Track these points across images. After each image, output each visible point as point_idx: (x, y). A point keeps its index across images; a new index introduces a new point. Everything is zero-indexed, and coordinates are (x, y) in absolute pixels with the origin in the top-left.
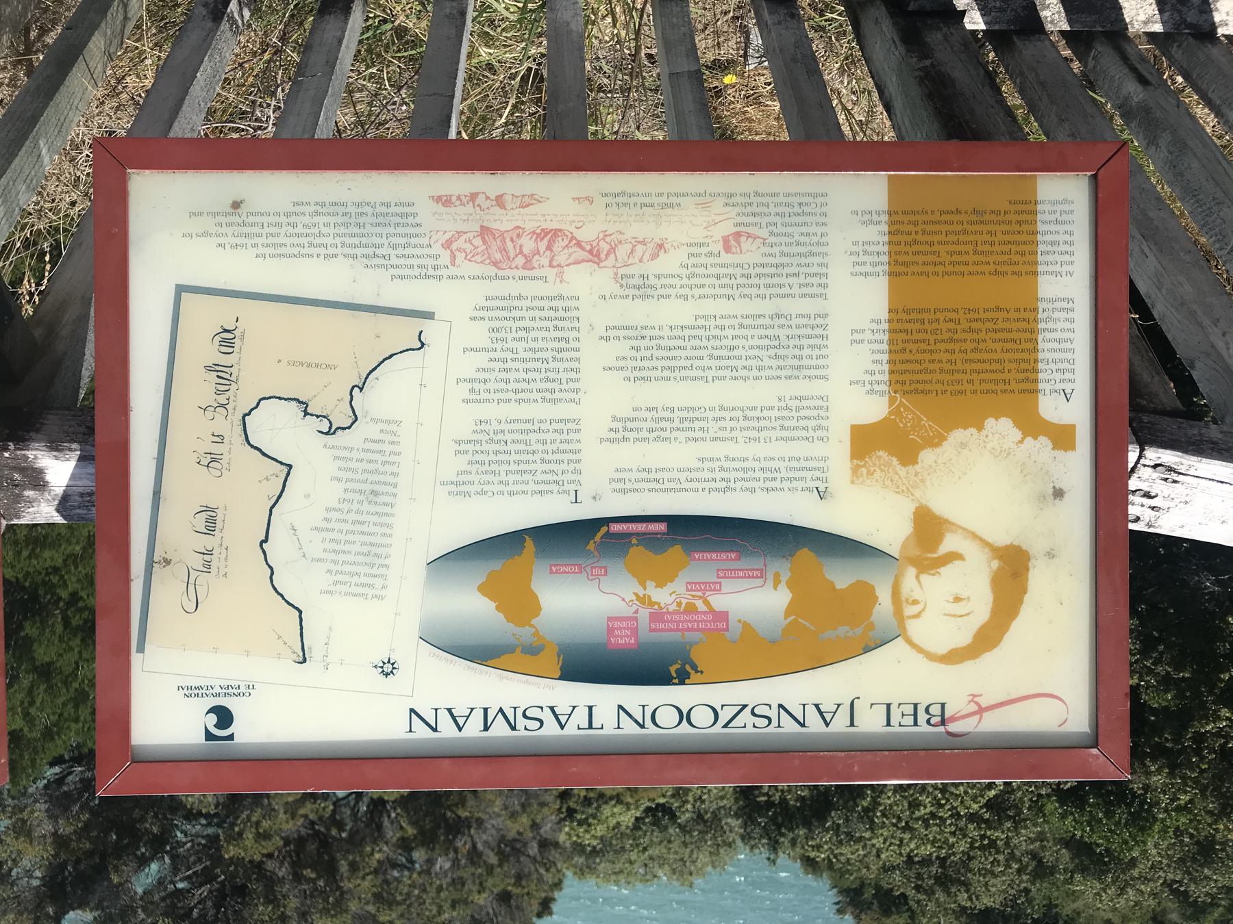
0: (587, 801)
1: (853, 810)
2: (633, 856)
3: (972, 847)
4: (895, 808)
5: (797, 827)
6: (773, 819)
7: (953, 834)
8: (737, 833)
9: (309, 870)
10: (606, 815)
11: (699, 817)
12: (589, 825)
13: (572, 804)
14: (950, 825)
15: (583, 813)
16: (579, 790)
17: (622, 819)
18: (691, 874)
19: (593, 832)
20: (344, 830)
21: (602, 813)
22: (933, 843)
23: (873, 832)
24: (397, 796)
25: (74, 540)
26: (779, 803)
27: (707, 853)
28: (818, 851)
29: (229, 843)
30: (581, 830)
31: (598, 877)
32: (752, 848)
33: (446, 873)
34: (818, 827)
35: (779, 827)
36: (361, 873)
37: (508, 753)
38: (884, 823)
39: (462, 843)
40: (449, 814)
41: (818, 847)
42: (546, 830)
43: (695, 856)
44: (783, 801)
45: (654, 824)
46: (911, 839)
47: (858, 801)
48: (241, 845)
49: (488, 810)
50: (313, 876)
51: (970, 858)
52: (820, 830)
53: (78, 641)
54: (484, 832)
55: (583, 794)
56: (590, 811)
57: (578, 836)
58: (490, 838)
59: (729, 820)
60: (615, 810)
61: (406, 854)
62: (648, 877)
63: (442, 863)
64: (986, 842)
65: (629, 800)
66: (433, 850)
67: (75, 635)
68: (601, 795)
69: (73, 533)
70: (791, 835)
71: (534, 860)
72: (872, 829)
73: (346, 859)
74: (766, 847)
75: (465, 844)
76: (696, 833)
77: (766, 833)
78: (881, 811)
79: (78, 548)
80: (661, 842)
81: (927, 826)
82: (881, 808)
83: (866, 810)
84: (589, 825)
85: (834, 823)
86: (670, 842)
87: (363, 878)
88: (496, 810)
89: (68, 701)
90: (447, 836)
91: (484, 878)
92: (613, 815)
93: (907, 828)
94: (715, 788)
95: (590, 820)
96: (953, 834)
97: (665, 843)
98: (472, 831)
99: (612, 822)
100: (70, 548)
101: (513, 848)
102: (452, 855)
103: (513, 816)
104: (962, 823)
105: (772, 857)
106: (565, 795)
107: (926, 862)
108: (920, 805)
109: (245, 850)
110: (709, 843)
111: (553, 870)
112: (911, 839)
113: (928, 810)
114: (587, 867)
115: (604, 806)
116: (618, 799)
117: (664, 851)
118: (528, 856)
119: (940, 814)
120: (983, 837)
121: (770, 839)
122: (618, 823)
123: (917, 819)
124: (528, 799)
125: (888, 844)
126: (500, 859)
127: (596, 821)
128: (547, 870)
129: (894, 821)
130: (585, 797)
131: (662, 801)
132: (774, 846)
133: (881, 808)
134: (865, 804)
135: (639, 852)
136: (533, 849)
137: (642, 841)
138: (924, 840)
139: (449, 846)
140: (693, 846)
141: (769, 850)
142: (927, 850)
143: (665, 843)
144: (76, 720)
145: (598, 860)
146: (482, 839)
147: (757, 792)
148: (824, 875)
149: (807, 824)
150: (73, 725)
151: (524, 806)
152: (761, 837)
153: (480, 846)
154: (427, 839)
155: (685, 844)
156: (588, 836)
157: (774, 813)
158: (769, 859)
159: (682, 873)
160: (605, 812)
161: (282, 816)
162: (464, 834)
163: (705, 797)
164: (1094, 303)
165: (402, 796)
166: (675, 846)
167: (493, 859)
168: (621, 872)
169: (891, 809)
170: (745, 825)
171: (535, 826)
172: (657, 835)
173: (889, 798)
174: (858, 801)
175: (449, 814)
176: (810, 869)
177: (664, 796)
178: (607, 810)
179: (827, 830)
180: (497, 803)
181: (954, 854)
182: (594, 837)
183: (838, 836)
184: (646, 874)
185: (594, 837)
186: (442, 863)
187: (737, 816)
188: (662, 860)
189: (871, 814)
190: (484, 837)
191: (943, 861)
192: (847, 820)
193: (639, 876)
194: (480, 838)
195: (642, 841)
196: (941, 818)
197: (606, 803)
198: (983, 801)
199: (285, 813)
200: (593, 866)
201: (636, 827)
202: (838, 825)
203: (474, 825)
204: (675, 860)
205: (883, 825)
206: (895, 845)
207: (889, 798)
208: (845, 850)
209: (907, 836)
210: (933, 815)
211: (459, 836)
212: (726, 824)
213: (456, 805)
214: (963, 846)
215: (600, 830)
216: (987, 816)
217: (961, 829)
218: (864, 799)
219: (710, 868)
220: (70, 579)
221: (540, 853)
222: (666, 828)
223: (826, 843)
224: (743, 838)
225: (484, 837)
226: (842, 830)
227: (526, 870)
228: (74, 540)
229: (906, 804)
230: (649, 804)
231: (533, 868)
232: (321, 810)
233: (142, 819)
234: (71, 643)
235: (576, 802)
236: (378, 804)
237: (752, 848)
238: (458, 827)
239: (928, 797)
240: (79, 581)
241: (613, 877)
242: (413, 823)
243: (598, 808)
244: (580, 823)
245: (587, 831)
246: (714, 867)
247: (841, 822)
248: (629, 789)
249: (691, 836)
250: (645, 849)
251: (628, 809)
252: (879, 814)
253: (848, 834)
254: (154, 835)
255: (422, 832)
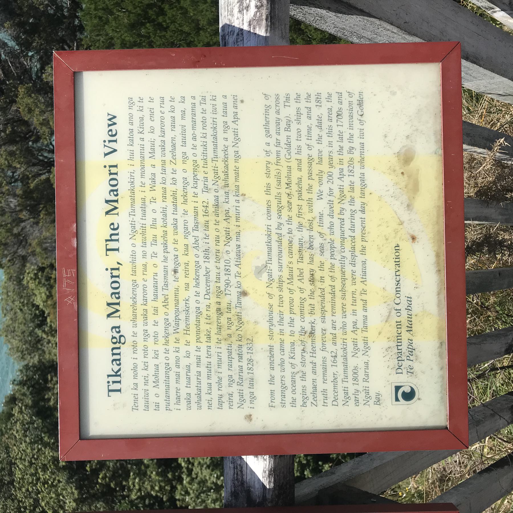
0: (48, 279)
1: (42, 432)
2: (17, 303)
3: (19, 501)
4: (43, 456)
5: (33, 397)
6: (38, 383)
7: (28, 490)
8: (29, 361)
9: (10, 130)
10: (41, 289)
11: (39, 341)
12: (35, 279)
13: (46, 271)
14: (33, 489)
15: (42, 276)
16: (55, 274)
17: (39, 298)
18: (6, 336)
19: (31, 282)
20: (33, 143)
21: (41, 287)
22: (23, 479)
23: (29, 443)
24: (52, 182)
25: (195, 12)
26: (46, 387)
27: (18, 345)
28: (19, 412)
29: (26, 88)
30: (32, 275)
31: (5, 283)
32: (21, 371)
33: (8, 205)
34: (33, 412)
35: (33, 386)
36: (9, 158)
37: (79, 282)
38: (34, 449)
39: (24, 215)
40: (42, 206)
41: (21, 412)
42: (31, 258)
43: (16, 338)
44: (49, 389)
45: (35, 314)
46: (25, 465)
47: (48, 434)
48: (24, 96)
49: (44, 228)
50: (7, 132)
51: (13, 500)
52: (31, 413)
53: (139, 12)
54: (31, 226)
55: (53, 276)
56: (43, 281)
57: (28, 273)
58: (28, 230)
59: (37, 357)
60: (43, 295)
61: (19, 179)
62: (5, 311)
63: (13, 202)
64: (22, 509)
65: (49, 302)
66: (22, 198)
67: (143, 11)
68: (51, 287)
69: (199, 12)
70: (28, 393)
71: (15, 252)
72: (31, 443)
73: (17, 150)
74: (22, 379)
75: (24, 216)
76: (30, 339)
77: (29, 379)
78: (41, 448)
79: (192, 14)
80: (25, 319)
81: (32, 475)
82: (43, 449)
83: (42, 439)
84: (35, 279)
85: (35, 421)
86: (25, 324)
87: (6, 159)
88: (44, 233)
89: (107, 5)
90: (29, 206)
91: (5, 228)
92: (40, 293)
93: (31, 463)
94: (57, 359)
95: (37, 280)
96: (28, 490)
97: (24, 322)
98: (32, 220)
99: (36, 292)
100: (191, 10)
101: (22, 241)
102: (18, 208)
103: (40, 244)
104: (33, 495)
105: (16, 382)
106: (52, 267)
107: (11, 474)
108: (45, 472)
109: (22, 98)
110: (24, 346)
111: (9, 264)
112: (25, 465)
113: (41, 476)
114: (11, 276)
115: (45, 288)
116: (50, 296)
117: (20, 321)
118: (18, 249)
119: (39, 484)
120: (25, 508)
121: (26, 381)
122: (36, 295)
123: (37, 469)
124: (49, 251)
125: (22, 452)
126: (16, 234)
127: (37, 283)
128: (9, 261)
129: (35, 456)
130: (51, 278)
131: (48, 320)
132: (22, 383)
133: (43, 449)
134: (46, 439)
135: (20, 306)
136: (21, 252)
137: (26, 308)
138: (24, 472)
139: (24, 207)
140: (22, 337)
141: (20, 381)
142: (18, 475)
143: (24, 322)
144: (95, 9)
145: (15, 283)
146: (27, 225)
147: (53, 374)
148: (5, 408)
149: (35, 404)
150: (93, 6)
151: (46, 249)
152: (27, 376)
153: (23, 224)
154: (27, 194)
155: (23, 332)
156: (29, 279)
157: (41, 383)
158: (14, 380)
159: (7, 331)
160: (42, 288)
161: (41, 118)
162: (29, 215)
163: (50, 345)
164: (288, 433)
165: (52, 185)
166: (22, 327)
167: (15, 231)
168: (8, 296)
169: (43, 454)
170: (34, 366)
171: (33, 253)
172: (29, 317)
173: (49, 453)
174: (48, 434)
175: (42, 206)
176: (7, 400)
177: (51, 322)
178: (43, 290)
179: (31, 418)
180: (48, 234)
181: (15, 491)
182: (28, 282)
183: (27, 424)
184: (6, 310)
185: (28, 282)
186: (13, 202)
187: (40, 361)
188: (14, 320)
189: (40, 442)
190: (28, 227)
191: (12, 482)
192: (36, 428)
193: (5, 306)
194: (28, 224)
195: (26, 308)
196: (37, 484)
197: (47, 289)
198: (46, 509)
199: (43, 120)
200: (12, 280)
201: (33, 305)
202: (33, 424)
203: (35, 220)
204: (14, 328)
205: (32, 449)
206: (22, 456)
207: (49, 453)
208: (18, 426)
209: (27, 464)
210: (38, 479)
211: (29, 213)
212: (35, 355)
213: (47, 210)
214: (20, 495)
215: (32, 285)
216: (37, 510)
217: (30, 494)
218: (49, 438)
219: (10, 346)
220: (174, 11)
221: (18, 256)
222: (33, 322)
223: (23, 417)
224: (27, 365)
225: (28, 227)
226: (31, 426)
227: (10, 249)
228: (195, 12)
229: (46, 462)
230: (47, 312)
231: (12, 251)
232: (44, 137)
233: (40, 38)
234: (138, 8)
235: (48, 272)
236: (49, 164)
237: (21, 371)
238: (34, 211)
239: (49, 476)
240: (173, 16)
241: (5, 291)
242: (37, 187)
243: (44, 285)
244: (36, 275)
245: (31, 278)
246: (10, 349)
247: (35, 425)
248: (55, 303)
249: (28, 336)
250: (21, 310)
251: (44, 302)
252: (40, 447)
253: (28, 429)
254: (32, 86)
255: (32, 192)
